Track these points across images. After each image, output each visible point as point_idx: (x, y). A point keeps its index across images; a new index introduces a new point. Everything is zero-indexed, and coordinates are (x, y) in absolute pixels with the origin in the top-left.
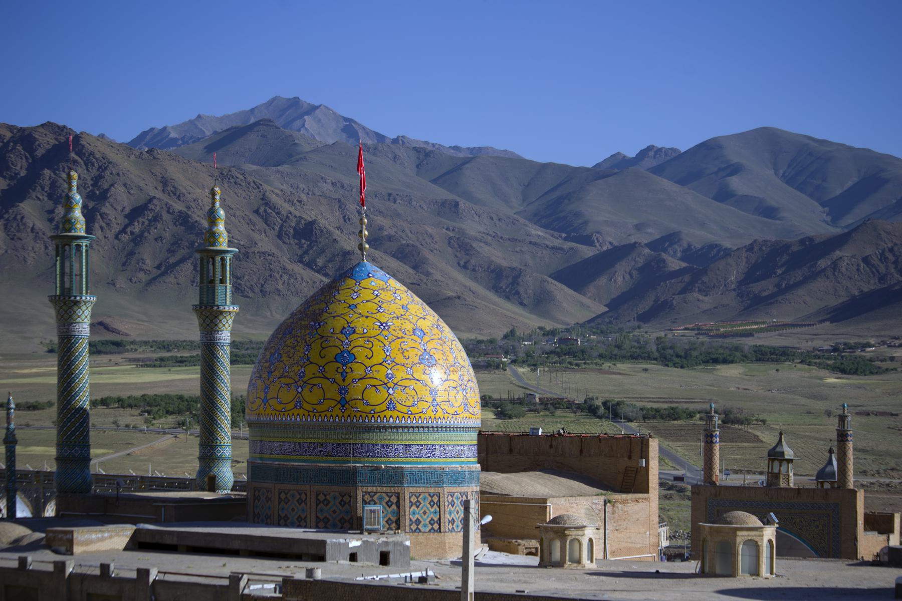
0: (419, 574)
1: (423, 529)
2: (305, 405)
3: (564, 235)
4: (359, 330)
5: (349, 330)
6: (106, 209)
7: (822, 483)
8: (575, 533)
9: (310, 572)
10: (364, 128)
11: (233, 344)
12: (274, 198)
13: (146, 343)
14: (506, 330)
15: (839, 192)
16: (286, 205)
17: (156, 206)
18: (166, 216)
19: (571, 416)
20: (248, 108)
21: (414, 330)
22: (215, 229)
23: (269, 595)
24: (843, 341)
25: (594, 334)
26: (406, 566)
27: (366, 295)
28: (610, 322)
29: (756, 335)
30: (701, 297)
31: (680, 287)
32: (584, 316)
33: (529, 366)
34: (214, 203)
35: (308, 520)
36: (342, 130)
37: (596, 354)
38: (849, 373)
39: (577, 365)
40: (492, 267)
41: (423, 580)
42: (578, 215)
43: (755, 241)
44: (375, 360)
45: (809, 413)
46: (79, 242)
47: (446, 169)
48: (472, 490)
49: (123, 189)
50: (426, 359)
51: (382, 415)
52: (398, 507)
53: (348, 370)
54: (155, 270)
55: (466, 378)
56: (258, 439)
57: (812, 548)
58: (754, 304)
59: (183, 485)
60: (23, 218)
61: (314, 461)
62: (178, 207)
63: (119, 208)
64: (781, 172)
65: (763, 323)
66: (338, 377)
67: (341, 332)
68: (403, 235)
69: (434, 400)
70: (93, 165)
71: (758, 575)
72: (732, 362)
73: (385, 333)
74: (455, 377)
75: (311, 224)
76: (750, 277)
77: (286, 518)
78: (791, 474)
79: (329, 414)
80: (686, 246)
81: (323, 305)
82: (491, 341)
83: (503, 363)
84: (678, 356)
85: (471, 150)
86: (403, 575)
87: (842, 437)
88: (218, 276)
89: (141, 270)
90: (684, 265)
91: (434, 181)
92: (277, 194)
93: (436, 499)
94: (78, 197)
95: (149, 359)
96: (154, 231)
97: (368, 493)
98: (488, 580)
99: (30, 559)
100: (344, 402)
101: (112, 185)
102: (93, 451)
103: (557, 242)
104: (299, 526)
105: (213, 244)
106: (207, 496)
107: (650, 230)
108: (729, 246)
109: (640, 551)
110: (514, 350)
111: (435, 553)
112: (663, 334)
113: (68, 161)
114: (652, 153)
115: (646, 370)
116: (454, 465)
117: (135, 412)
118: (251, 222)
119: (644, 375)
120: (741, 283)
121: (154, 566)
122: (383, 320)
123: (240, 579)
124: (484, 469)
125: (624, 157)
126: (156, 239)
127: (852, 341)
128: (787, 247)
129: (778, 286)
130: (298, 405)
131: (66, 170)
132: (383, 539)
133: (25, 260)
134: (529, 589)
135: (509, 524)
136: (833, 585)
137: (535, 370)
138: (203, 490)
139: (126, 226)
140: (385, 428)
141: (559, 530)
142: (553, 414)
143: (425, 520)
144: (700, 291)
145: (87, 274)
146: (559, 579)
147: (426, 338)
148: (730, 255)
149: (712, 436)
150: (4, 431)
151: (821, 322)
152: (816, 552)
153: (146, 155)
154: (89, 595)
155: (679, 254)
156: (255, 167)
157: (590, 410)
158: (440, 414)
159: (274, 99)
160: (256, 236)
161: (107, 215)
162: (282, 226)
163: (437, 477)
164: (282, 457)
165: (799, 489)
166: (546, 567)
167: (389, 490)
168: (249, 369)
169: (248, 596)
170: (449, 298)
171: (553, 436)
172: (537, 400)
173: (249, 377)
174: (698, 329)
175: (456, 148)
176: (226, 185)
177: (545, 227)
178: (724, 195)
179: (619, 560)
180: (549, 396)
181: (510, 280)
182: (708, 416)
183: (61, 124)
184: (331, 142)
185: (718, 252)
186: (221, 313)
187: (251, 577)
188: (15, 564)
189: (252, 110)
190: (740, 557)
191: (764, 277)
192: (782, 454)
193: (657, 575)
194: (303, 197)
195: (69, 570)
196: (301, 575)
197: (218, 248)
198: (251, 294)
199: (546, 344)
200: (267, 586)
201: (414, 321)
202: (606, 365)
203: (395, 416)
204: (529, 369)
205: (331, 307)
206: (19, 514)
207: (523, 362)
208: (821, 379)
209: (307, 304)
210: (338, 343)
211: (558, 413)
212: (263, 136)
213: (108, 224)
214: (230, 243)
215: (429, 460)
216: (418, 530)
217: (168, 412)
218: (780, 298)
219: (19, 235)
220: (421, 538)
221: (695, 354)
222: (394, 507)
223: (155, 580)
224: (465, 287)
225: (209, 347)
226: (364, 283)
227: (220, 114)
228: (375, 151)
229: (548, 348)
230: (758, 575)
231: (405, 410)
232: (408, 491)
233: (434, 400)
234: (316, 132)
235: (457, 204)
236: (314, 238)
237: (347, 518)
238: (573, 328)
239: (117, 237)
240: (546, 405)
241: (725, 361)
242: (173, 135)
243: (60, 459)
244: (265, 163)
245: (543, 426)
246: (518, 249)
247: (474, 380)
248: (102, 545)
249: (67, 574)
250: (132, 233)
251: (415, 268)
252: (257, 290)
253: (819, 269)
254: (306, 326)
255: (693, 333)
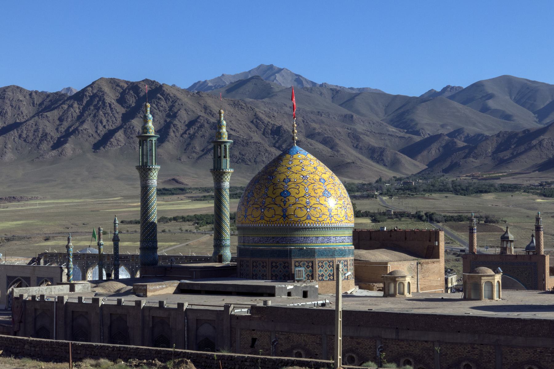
0: (321, 302)
1: (325, 279)
2: (265, 218)
3: (406, 131)
4: (292, 180)
5: (287, 180)
6: (176, 122)
7: (528, 252)
8: (401, 280)
9: (265, 302)
10: (306, 79)
11: (231, 189)
12: (261, 115)
13: (197, 189)
14: (377, 179)
15: (542, 106)
16: (267, 119)
17: (201, 120)
18: (206, 125)
19: (409, 221)
20: (247, 70)
21: (320, 179)
22: (221, 131)
23: (244, 315)
24: (545, 180)
25: (421, 179)
26: (316, 298)
27: (296, 162)
28: (429, 174)
29: (502, 178)
30: (474, 160)
31: (463, 155)
32: (416, 171)
33: (388, 196)
34: (220, 118)
35: (267, 275)
36: (295, 81)
37: (422, 189)
38: (548, 197)
39: (412, 195)
40: (370, 147)
41: (323, 305)
42: (412, 120)
43: (501, 132)
44: (300, 195)
45: (528, 217)
46: (151, 139)
47: (346, 99)
48: (350, 258)
49: (184, 112)
50: (326, 194)
51: (304, 222)
52: (312, 268)
53: (287, 200)
54: (201, 152)
55: (346, 203)
56: (242, 236)
57: (523, 284)
58: (500, 163)
59: (207, 260)
60: (133, 127)
61: (270, 246)
62: (213, 120)
63: (183, 122)
64: (513, 97)
65: (505, 172)
66: (282, 204)
67: (283, 181)
68: (325, 132)
69: (330, 214)
70: (169, 100)
71: (493, 299)
72: (489, 192)
73: (305, 181)
74: (341, 202)
75: (279, 128)
76: (498, 150)
77: (256, 275)
78: (513, 248)
79: (277, 222)
80: (466, 135)
81: (274, 168)
82: (370, 184)
83: (376, 195)
84: (462, 190)
85: (359, 89)
86: (313, 303)
87: (538, 229)
88: (223, 155)
89: (194, 152)
90: (465, 144)
91: (341, 105)
92: (262, 113)
93: (331, 264)
94: (150, 116)
95: (198, 197)
96: (200, 133)
97: (297, 261)
98: (357, 304)
99: (123, 300)
100: (285, 216)
101: (179, 110)
102: (159, 244)
103: (402, 134)
104: (263, 279)
105: (220, 138)
106: (217, 265)
107: (448, 127)
108: (488, 135)
109: (436, 287)
110: (381, 188)
111: (331, 291)
112: (455, 179)
113: (156, 98)
114: (449, 89)
115: (446, 197)
116: (340, 246)
117: (191, 223)
118: (249, 127)
119: (445, 199)
120: (494, 153)
121: (187, 301)
122: (305, 175)
123: (229, 307)
124: (356, 248)
125: (435, 91)
126: (201, 137)
127: (549, 181)
128: (517, 134)
129: (512, 154)
130: (262, 218)
131: (156, 103)
132: (304, 285)
133: (135, 148)
134: (375, 308)
135: (365, 276)
136: (530, 304)
137: (391, 198)
138: (216, 262)
139: (186, 131)
140: (306, 228)
141: (393, 278)
142: (400, 220)
143: (326, 274)
144: (474, 157)
145: (155, 155)
146: (392, 303)
147: (326, 183)
148: (488, 139)
149: (473, 229)
150: (113, 235)
151: (534, 171)
152: (526, 287)
153: (196, 95)
154: (153, 317)
155: (463, 139)
156: (251, 100)
157: (418, 217)
158: (333, 221)
159: (260, 66)
160: (252, 134)
161: (177, 125)
162: (264, 130)
163: (332, 253)
164: (254, 244)
165: (516, 255)
166: (386, 297)
167: (308, 260)
168: (238, 200)
169: (234, 315)
170: (349, 163)
171: (391, 231)
172: (392, 213)
173: (237, 205)
174: (473, 176)
175: (352, 88)
176: (236, 109)
177: (396, 127)
178: (485, 109)
179: (425, 293)
180: (398, 211)
181: (379, 153)
182: (470, 219)
183: (152, 79)
184: (289, 86)
185: (482, 138)
186: (225, 173)
187: (235, 306)
188: (115, 303)
189: (250, 72)
190: (483, 291)
191: (506, 149)
192: (508, 238)
193: (442, 300)
194: (275, 114)
195: (143, 305)
196: (261, 304)
197: (223, 140)
198: (249, 163)
199: (397, 185)
200: (243, 310)
201: (320, 175)
202: (427, 195)
203: (310, 223)
204: (388, 197)
205: (278, 169)
206: (121, 277)
207: (386, 194)
208: (534, 200)
209: (266, 167)
210: (282, 187)
211: (403, 219)
212: (256, 84)
213: (177, 130)
214: (229, 138)
215: (328, 244)
216: (323, 280)
217: (207, 223)
218: (513, 160)
219: (131, 136)
220: (324, 283)
221: (471, 188)
222: (310, 268)
223: (187, 309)
224: (357, 157)
225: (219, 190)
226: (295, 156)
227: (233, 74)
228: (311, 90)
229: (398, 187)
230: (493, 299)
231: (316, 219)
232: (317, 260)
233: (330, 214)
234: (281, 82)
235: (352, 117)
236: (281, 134)
237: (287, 275)
238: (410, 177)
239: (181, 136)
240: (397, 215)
241: (486, 192)
242: (210, 84)
243: (142, 248)
244: (256, 98)
245: (404, 225)
246: (383, 138)
247: (351, 204)
248: (162, 292)
249: (142, 307)
250: (189, 134)
251: (331, 148)
252: (253, 161)
253: (532, 145)
254: (266, 179)
255: (470, 178)
